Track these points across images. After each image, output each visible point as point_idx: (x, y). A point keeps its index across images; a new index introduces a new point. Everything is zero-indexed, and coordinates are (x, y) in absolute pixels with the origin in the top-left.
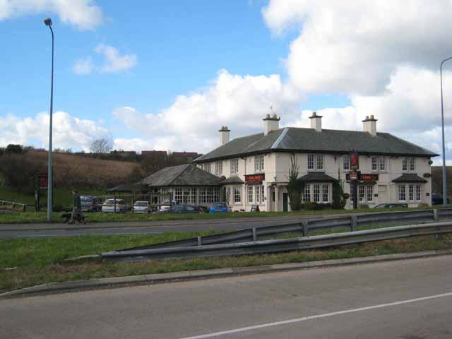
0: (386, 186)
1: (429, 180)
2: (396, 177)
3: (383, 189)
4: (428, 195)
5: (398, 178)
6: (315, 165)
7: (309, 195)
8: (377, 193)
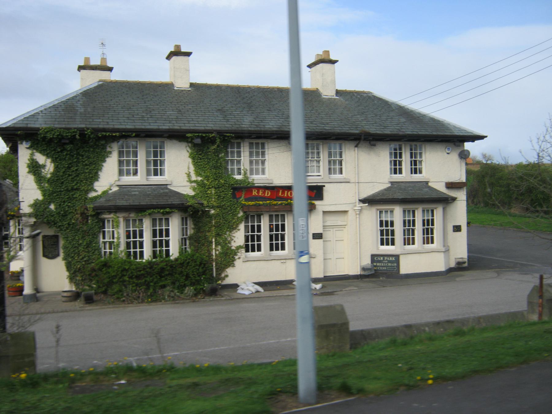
0: (346, 212)
1: (461, 196)
2: (369, 191)
3: (331, 220)
4: (457, 229)
5: (374, 195)
6: (406, 165)
7: (393, 232)
8: (319, 231)
